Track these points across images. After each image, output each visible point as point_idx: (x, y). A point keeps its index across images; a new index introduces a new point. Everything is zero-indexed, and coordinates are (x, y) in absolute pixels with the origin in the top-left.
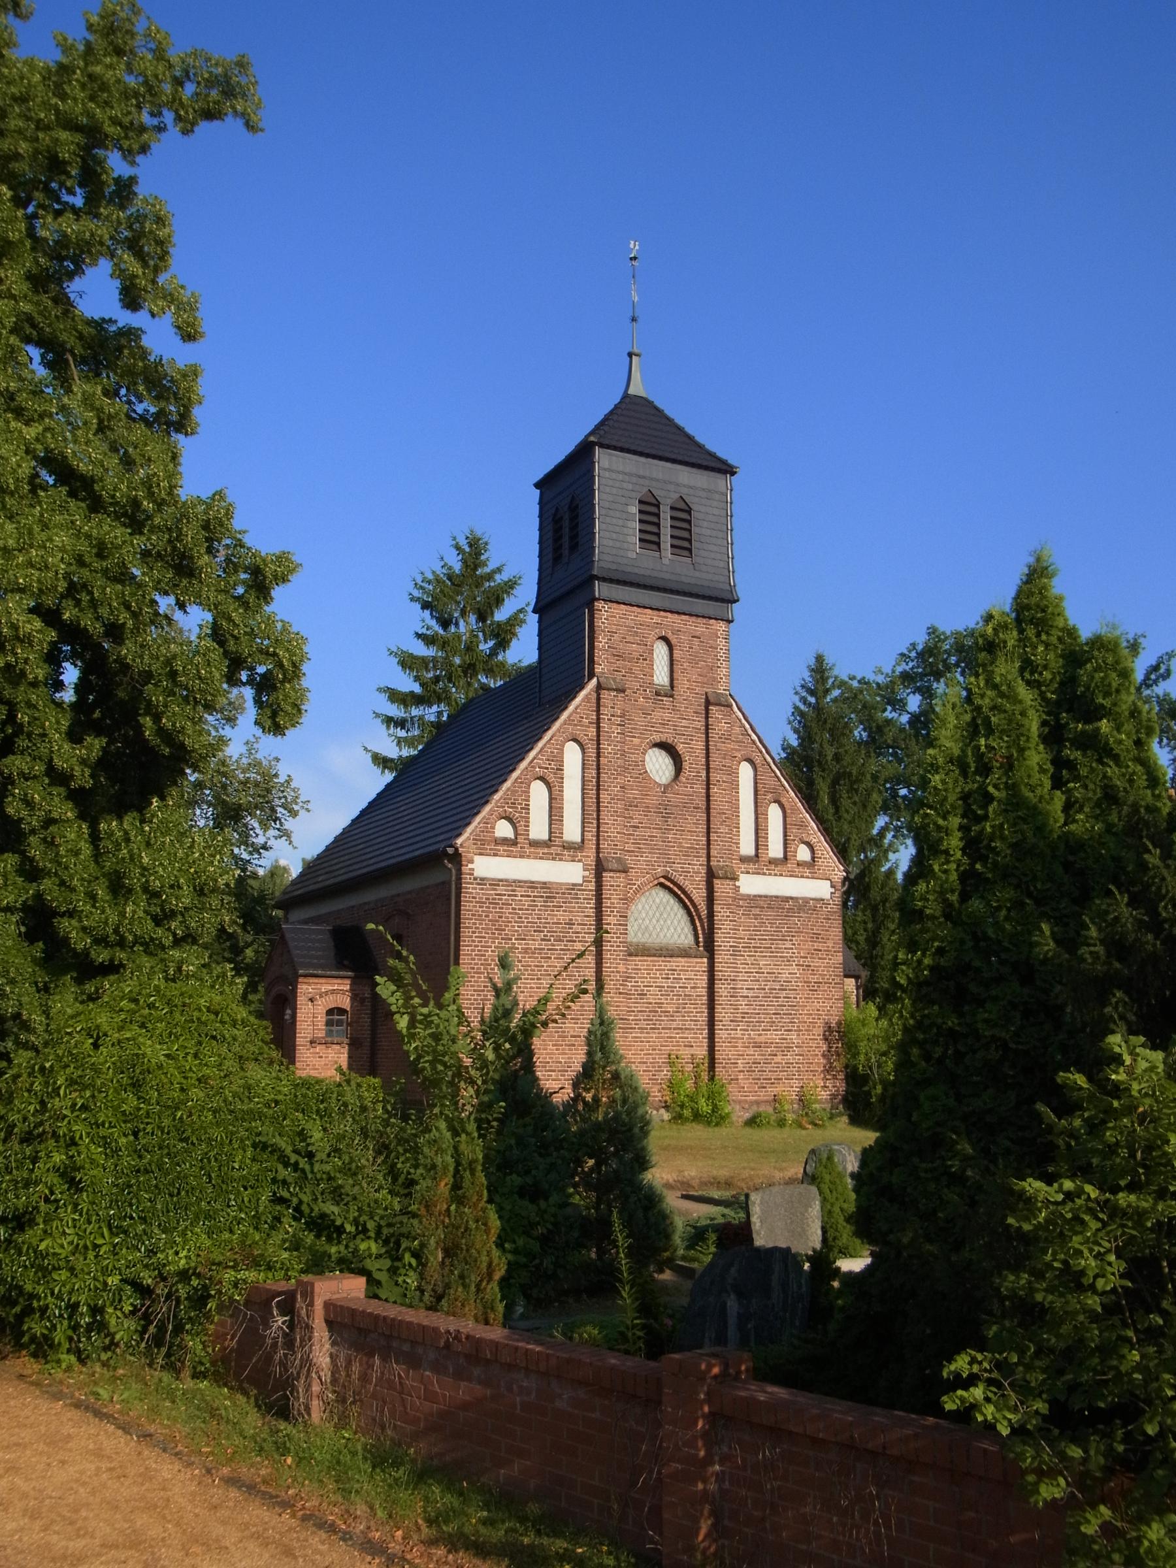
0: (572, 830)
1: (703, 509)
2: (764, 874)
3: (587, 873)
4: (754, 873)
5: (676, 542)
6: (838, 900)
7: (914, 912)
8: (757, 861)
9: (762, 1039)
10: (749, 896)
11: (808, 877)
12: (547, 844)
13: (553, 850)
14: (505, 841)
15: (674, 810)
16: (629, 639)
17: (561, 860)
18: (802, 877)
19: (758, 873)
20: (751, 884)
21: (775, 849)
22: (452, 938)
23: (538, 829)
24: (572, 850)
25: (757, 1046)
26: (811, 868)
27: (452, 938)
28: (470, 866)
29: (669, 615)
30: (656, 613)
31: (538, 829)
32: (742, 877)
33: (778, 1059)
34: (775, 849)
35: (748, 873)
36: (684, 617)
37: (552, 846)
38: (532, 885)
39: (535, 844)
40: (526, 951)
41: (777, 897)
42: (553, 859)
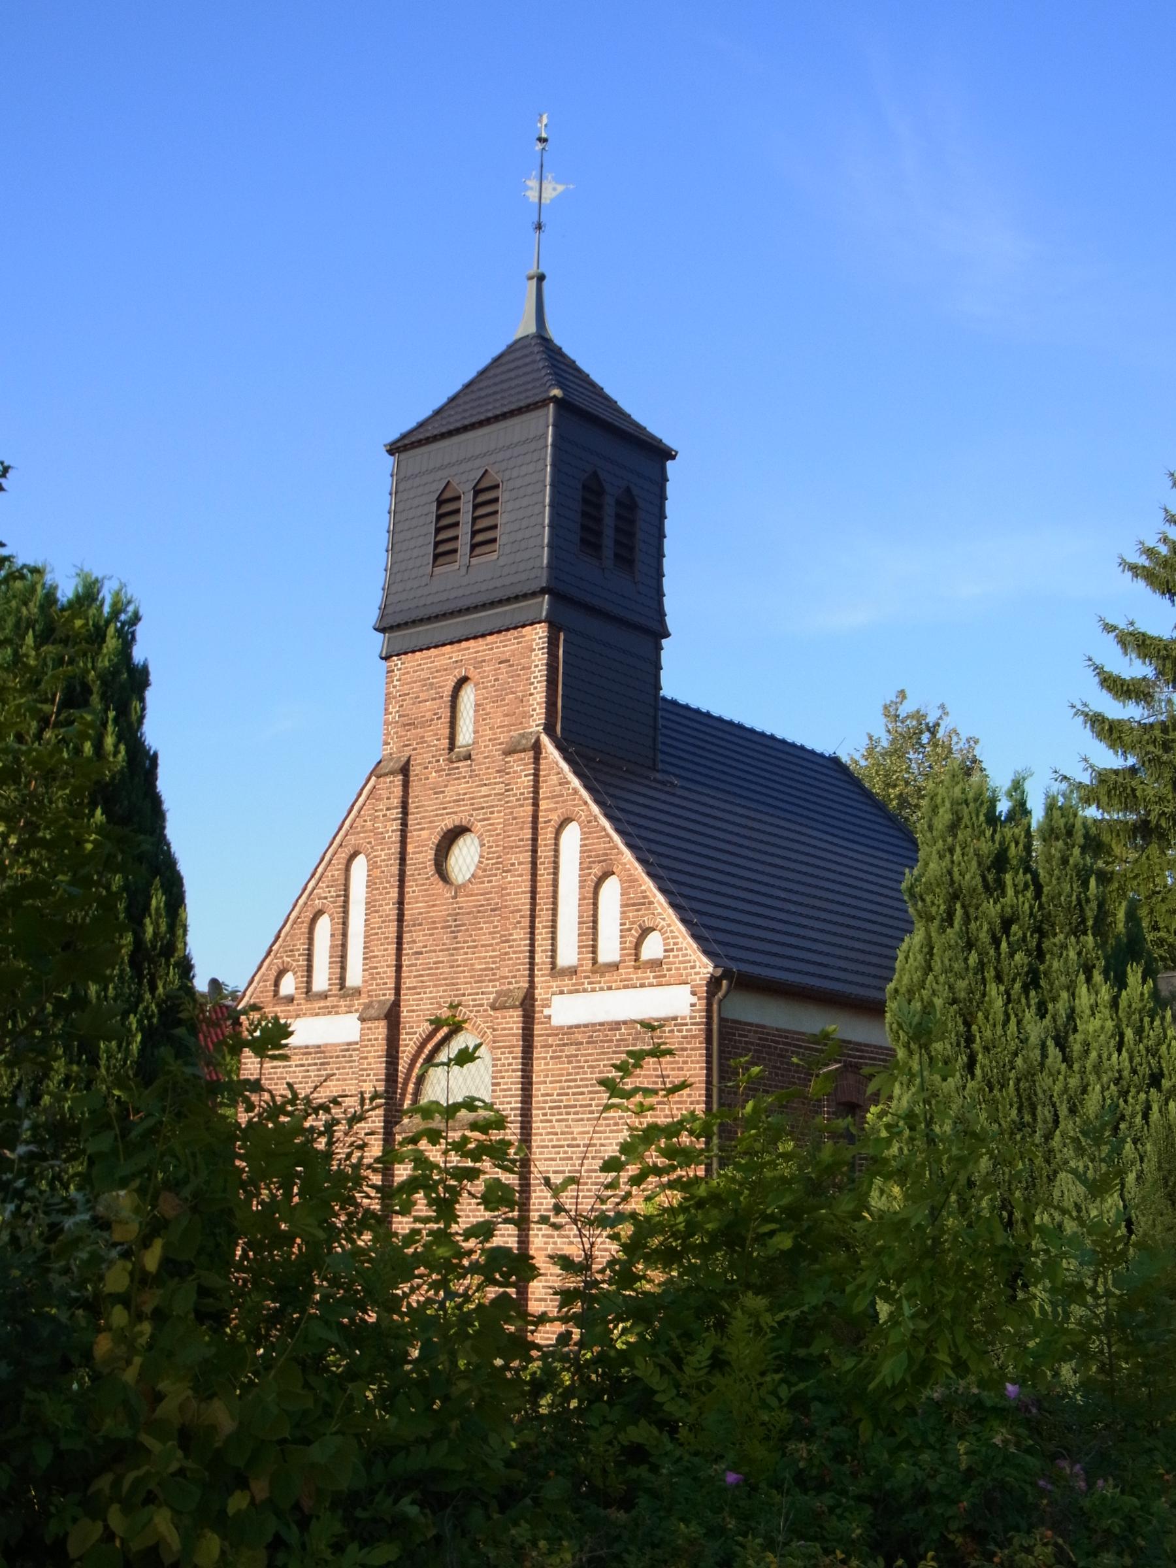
1: (507, 475)
2: (585, 991)
3: (546, 1012)
4: (570, 992)
6: (700, 1017)
8: (595, 972)
10: (562, 1028)
11: (651, 985)
14: (656, 964)
15: (466, 919)
16: (423, 696)
17: (337, 1013)
18: (642, 986)
19: (577, 991)
21: (610, 949)
22: (715, 1027)
26: (637, 967)
27: (715, 1027)
28: (546, 1012)
29: (472, 643)
30: (456, 646)
34: (610, 949)
35: (562, 993)
36: (489, 638)
41: (601, 1024)
42: (330, 1013)
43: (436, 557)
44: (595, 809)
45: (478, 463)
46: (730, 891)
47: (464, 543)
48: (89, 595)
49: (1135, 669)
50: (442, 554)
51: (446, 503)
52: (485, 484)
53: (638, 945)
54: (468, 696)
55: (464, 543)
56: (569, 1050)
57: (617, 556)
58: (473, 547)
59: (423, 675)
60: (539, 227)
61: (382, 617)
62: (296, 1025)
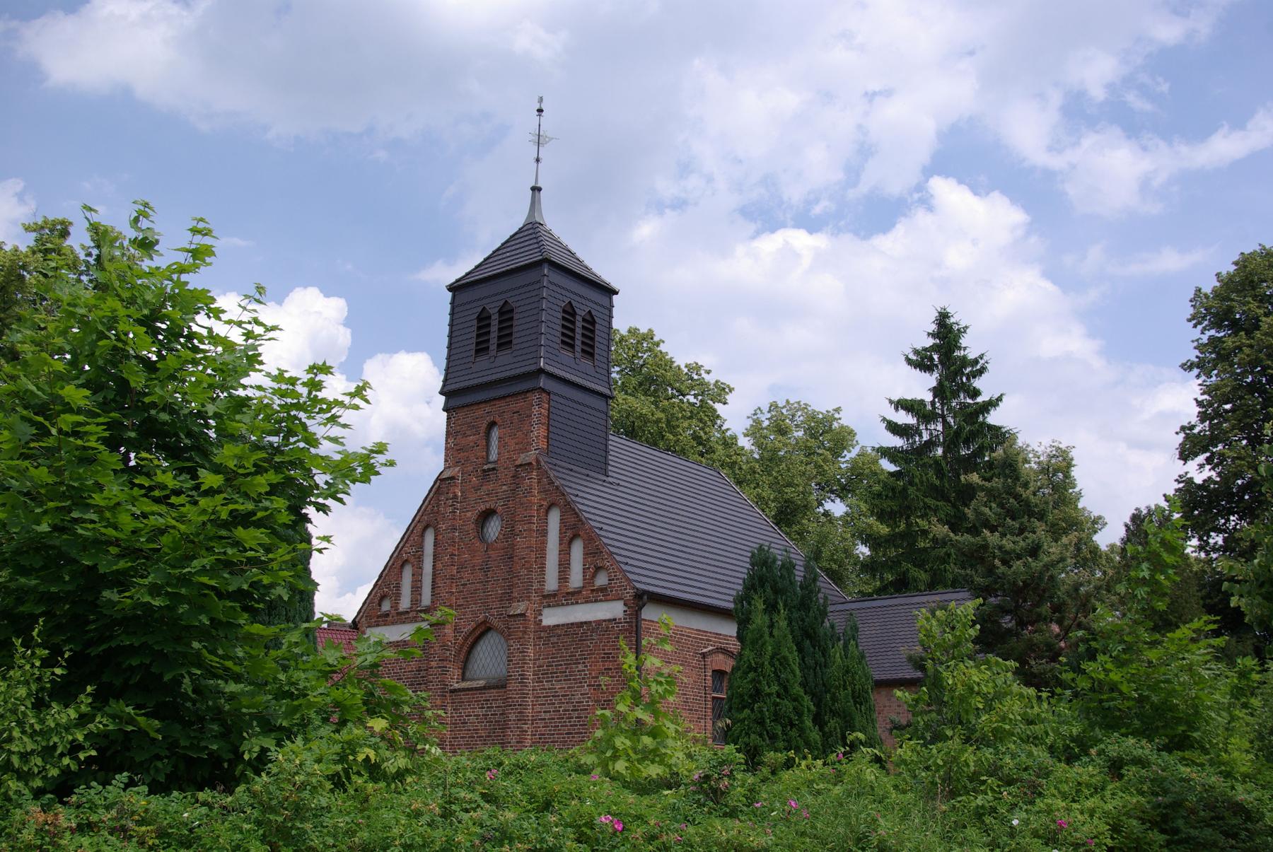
8: (553, 599)
14: (602, 589)
18: (596, 601)
20: (552, 617)
21: (576, 579)
34: (576, 579)
43: (477, 351)
44: (889, 677)
45: (480, 303)
46: (696, 571)
47: (494, 341)
48: (1236, 263)
49: (904, 418)
50: (481, 349)
51: (483, 318)
52: (484, 315)
53: (594, 576)
54: (495, 434)
55: (494, 341)
56: (554, 640)
57: (583, 351)
58: (499, 346)
59: (469, 420)
60: (538, 160)
61: (444, 386)
62: (338, 376)
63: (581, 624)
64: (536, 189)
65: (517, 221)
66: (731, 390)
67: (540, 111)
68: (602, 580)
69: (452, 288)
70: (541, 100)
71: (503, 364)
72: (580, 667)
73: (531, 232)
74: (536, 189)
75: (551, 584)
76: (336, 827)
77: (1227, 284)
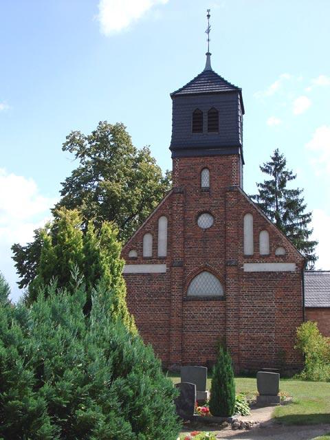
0: (163, 251)
5: (205, 126)
7: (81, 201)
8: (256, 257)
9: (255, 336)
12: (150, 258)
13: (153, 260)
14: (280, 256)
20: (249, 268)
21: (264, 248)
23: (147, 252)
24: (161, 260)
25: (253, 339)
31: (147, 252)
32: (245, 265)
33: (264, 345)
34: (264, 248)
35: (248, 262)
37: (155, 259)
38: (143, 275)
39: (146, 259)
40: (140, 301)
63: (270, 273)
64: (208, 54)
65: (201, 69)
66: (16, 248)
67: (209, 16)
68: (280, 252)
69: (174, 96)
70: (208, 11)
71: (206, 136)
72: (270, 293)
73: (209, 75)
74: (208, 54)
75: (248, 249)
76: (70, 301)
77: (33, 246)
